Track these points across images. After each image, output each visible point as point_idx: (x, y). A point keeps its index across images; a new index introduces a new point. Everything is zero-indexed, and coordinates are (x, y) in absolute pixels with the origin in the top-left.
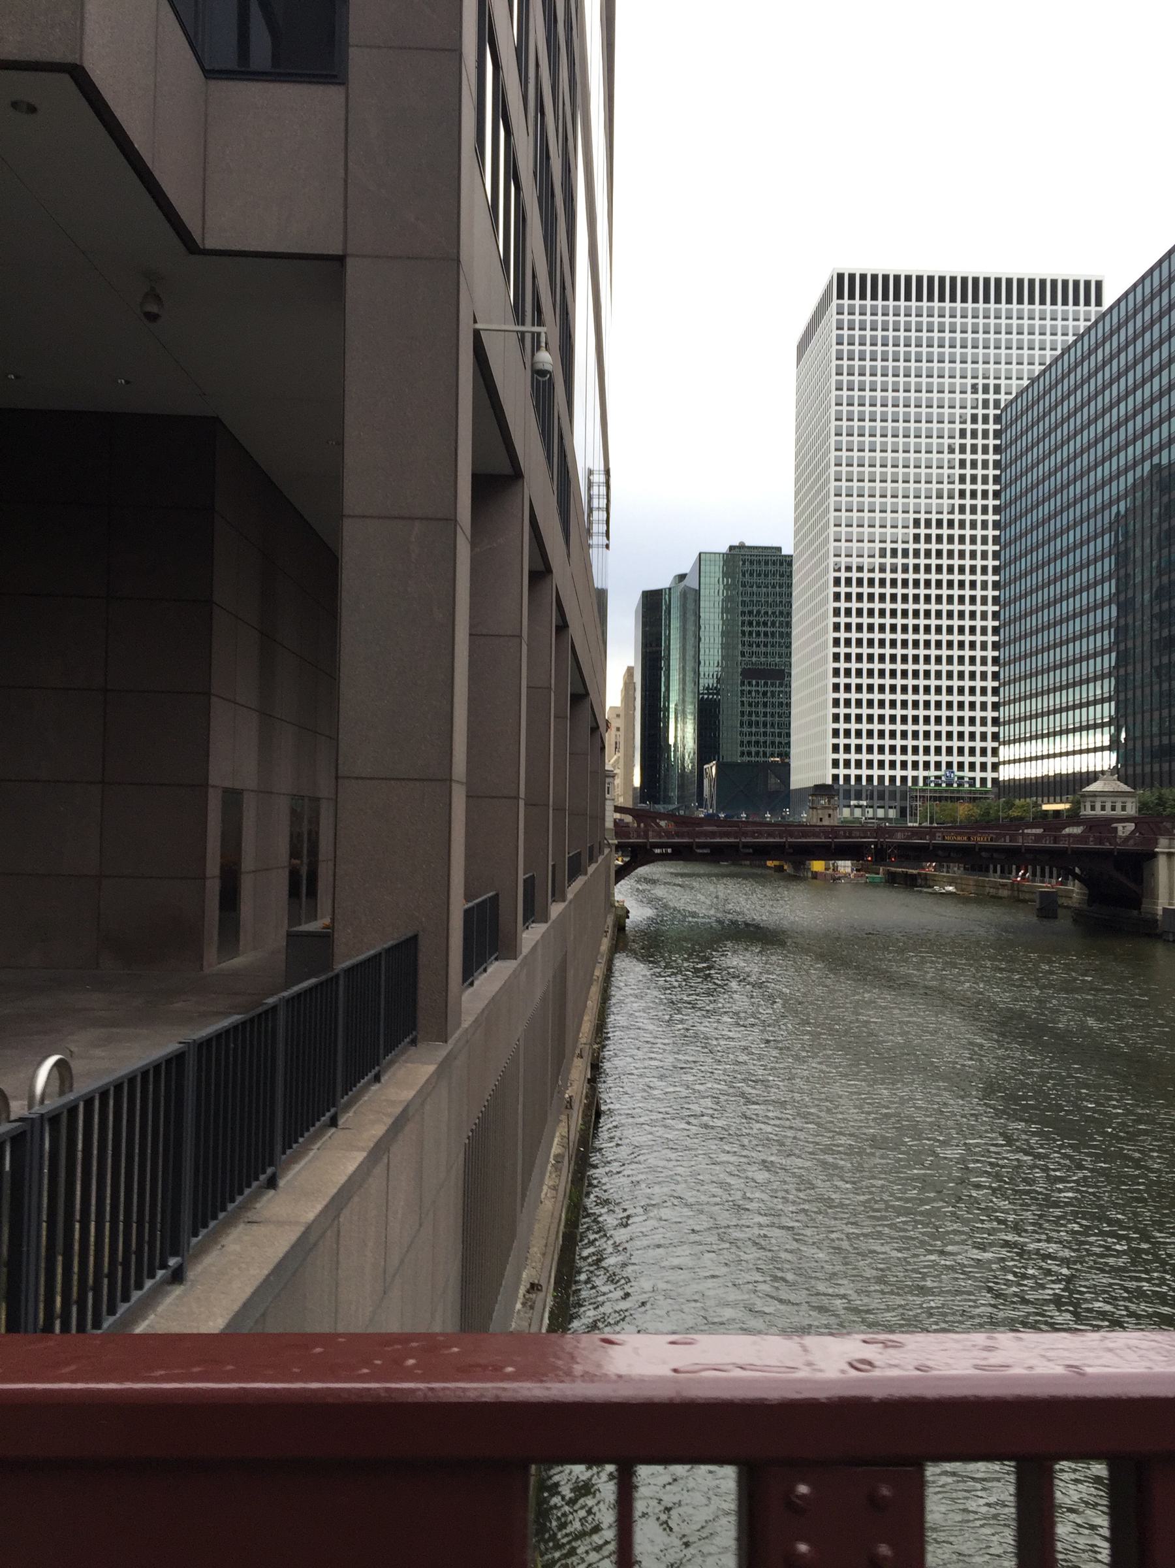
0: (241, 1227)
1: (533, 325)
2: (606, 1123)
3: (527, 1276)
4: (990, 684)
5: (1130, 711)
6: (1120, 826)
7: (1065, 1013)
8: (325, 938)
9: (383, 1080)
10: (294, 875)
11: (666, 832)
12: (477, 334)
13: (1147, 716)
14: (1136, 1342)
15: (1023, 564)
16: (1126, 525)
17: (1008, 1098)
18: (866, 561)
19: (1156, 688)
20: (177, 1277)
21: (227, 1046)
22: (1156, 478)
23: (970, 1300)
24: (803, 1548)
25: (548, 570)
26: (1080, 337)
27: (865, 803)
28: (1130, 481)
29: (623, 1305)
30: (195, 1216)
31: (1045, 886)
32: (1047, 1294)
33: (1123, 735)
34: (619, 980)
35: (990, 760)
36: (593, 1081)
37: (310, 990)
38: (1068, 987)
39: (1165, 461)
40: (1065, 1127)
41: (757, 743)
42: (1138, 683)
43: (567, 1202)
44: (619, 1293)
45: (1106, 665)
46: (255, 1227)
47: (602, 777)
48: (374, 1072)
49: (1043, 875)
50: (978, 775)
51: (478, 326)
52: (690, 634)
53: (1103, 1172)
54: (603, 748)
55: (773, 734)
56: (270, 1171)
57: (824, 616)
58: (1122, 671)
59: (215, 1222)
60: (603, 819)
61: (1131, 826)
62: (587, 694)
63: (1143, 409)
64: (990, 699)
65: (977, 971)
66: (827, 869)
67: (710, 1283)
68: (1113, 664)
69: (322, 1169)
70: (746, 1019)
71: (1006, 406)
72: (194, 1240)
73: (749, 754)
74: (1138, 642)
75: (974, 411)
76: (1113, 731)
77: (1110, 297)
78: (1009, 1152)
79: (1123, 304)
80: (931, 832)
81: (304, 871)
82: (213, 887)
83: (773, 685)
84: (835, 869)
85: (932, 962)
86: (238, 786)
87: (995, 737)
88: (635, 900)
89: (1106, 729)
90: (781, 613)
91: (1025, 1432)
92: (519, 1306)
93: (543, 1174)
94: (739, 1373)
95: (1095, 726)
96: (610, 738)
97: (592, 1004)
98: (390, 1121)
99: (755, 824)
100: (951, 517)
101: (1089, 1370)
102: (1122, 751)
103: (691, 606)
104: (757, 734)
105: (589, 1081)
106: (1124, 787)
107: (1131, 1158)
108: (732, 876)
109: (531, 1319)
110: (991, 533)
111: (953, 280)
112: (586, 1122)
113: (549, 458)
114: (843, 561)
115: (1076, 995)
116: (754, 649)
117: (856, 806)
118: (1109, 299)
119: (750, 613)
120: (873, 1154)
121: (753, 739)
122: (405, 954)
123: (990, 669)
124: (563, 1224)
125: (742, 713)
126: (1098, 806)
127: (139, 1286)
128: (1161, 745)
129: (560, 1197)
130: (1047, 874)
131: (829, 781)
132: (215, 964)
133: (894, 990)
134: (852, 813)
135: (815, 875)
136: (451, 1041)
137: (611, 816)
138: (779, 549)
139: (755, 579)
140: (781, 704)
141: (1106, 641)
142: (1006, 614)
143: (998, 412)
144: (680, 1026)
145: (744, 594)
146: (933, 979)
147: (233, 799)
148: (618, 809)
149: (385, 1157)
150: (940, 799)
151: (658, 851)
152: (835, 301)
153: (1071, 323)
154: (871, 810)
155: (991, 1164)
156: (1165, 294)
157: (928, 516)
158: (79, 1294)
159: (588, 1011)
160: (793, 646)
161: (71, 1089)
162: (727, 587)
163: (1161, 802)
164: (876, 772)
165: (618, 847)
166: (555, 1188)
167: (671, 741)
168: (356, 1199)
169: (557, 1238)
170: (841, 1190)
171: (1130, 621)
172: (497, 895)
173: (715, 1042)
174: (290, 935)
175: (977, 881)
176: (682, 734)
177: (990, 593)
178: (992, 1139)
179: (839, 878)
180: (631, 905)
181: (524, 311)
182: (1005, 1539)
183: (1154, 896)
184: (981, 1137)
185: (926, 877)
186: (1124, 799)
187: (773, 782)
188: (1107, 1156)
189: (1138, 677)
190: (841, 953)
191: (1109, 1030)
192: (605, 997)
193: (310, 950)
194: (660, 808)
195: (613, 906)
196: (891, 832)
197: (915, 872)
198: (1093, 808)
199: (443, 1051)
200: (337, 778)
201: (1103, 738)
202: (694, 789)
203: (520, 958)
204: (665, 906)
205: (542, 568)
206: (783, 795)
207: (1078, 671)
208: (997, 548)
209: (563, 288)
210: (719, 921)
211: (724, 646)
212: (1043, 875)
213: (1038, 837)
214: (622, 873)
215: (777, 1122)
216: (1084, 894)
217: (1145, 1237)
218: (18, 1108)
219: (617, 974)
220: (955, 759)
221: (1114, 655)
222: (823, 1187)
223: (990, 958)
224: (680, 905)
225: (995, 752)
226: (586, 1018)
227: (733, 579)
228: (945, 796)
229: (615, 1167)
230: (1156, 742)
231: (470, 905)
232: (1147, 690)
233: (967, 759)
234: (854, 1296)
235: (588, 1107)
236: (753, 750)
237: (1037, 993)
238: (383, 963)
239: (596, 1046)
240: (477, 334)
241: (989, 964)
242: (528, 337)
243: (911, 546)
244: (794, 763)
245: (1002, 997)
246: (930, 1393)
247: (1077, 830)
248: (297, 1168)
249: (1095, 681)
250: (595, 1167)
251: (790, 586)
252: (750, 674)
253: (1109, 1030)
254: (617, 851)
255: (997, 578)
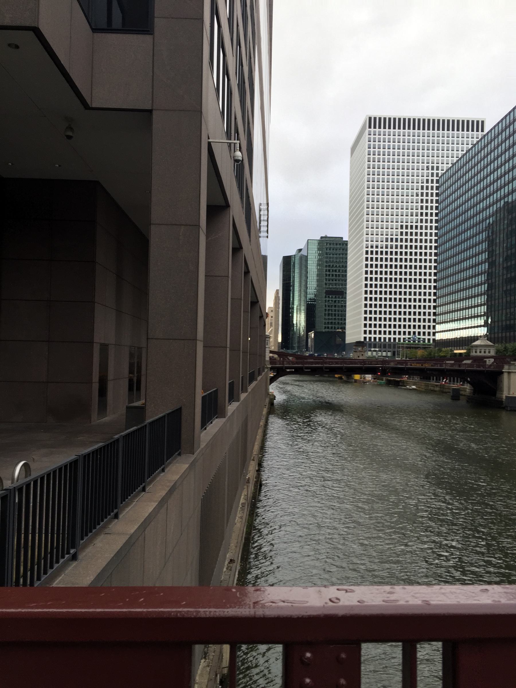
0: (102, 536)
1: (235, 140)
2: (264, 489)
3: (229, 556)
4: (433, 297)
5: (493, 309)
6: (487, 360)
7: (462, 441)
8: (142, 409)
9: (166, 471)
10: (131, 381)
11: (292, 362)
12: (209, 144)
13: (500, 312)
14: (454, 590)
15: (448, 245)
16: (493, 228)
17: (437, 479)
18: (379, 243)
19: (504, 300)
20: (74, 557)
21: (97, 456)
22: (506, 208)
23: (418, 566)
24: (308, 680)
25: (241, 248)
26: (474, 145)
27: (377, 349)
28: (495, 209)
29: (271, 568)
30: (82, 530)
31: (455, 386)
32: (451, 563)
33: (490, 320)
34: (270, 427)
35: (432, 331)
36: (259, 471)
37: (134, 432)
38: (464, 430)
39: (510, 200)
40: (460, 490)
41: (332, 323)
42: (497, 297)
43: (246, 524)
44: (268, 563)
45: (483, 290)
46: (108, 536)
47: (264, 338)
48: (162, 468)
49: (454, 381)
50: (427, 337)
51: (210, 140)
52: (303, 275)
53: (477, 511)
54: (265, 325)
55: (338, 319)
56: (115, 511)
57: (361, 268)
58: (490, 293)
59: (91, 534)
60: (265, 356)
61: (492, 360)
62: (258, 302)
63: (501, 177)
64: (432, 304)
65: (425, 422)
66: (361, 378)
67: (307, 559)
68: (486, 289)
69: (139, 510)
70: (325, 444)
71: (441, 176)
72: (82, 542)
73: (328, 328)
74: (497, 279)
75: (428, 178)
76: (485, 319)
77: (487, 128)
78: (436, 501)
79: (493, 131)
80: (405, 362)
81: (135, 379)
82: (96, 386)
83: (339, 298)
84: (364, 378)
85: (405, 419)
86: (106, 342)
87: (434, 320)
88: (278, 392)
89: (482, 318)
90: (343, 266)
91: (406, 629)
92: (225, 569)
93: (236, 511)
94: (282, 604)
95: (478, 316)
96: (268, 321)
97: (259, 437)
98: (168, 489)
99: (330, 358)
100: (417, 224)
101: (432, 602)
102: (489, 327)
103: (304, 262)
104: (331, 319)
105: (257, 471)
106: (490, 343)
107: (489, 505)
108: (320, 381)
109: (230, 575)
110: (434, 231)
111: (419, 120)
112: (255, 489)
113: (242, 198)
114: (370, 243)
115: (466, 432)
116: (331, 282)
117: (374, 351)
118: (487, 129)
119: (329, 266)
120: (378, 503)
121: (330, 321)
122: (176, 416)
123: (433, 291)
124: (244, 533)
125: (325, 310)
126: (478, 351)
127: (57, 562)
128: (506, 325)
129: (244, 521)
130: (456, 381)
131: (362, 340)
132: (96, 420)
133: (389, 431)
134: (372, 354)
135: (356, 381)
136: (196, 454)
137: (268, 355)
138: (342, 238)
139: (331, 251)
140: (342, 306)
141: (483, 279)
142: (440, 267)
143: (438, 178)
144: (297, 447)
145: (327, 258)
146: (405, 426)
147: (104, 348)
148: (271, 352)
149: (166, 505)
150: (410, 348)
151: (288, 370)
152: (368, 129)
153: (470, 139)
154: (380, 352)
155: (428, 507)
156: (512, 127)
157: (412, 224)
158: (31, 566)
159: (257, 440)
160: (348, 281)
161: (30, 475)
162: (319, 255)
163: (506, 349)
164: (397, 336)
165: (271, 369)
166: (241, 518)
167: (295, 322)
168: (152, 523)
169: (242, 539)
170: (363, 518)
171: (494, 270)
172: (217, 390)
173: (311, 454)
174: (128, 408)
175: (426, 384)
176: (299, 319)
177: (433, 258)
178: (429, 496)
179: (366, 382)
180: (276, 393)
181: (231, 133)
182: (398, 677)
183: (502, 391)
184: (424, 495)
185: (403, 382)
186: (489, 348)
187: (339, 340)
188: (479, 503)
189: (497, 295)
190: (367, 415)
191: (481, 449)
192: (265, 434)
193: (136, 414)
194: (290, 351)
195: (269, 394)
196: (388, 362)
197: (399, 380)
198: (476, 352)
199: (192, 458)
200: (147, 339)
201: (481, 321)
202: (304, 343)
203: (227, 417)
204: (291, 395)
205: (237, 246)
206: (342, 346)
207: (470, 292)
208: (436, 238)
209: (249, 123)
210: (314, 401)
211: (318, 281)
212: (454, 381)
213: (452, 365)
214: (273, 380)
215: (338, 489)
216: (471, 390)
217: (494, 539)
218: (7, 484)
219: (270, 424)
220: (417, 330)
221: (486, 285)
222: (356, 516)
223: (430, 417)
224: (297, 394)
225: (434, 327)
226: (256, 443)
227: (322, 251)
228: (412, 346)
229: (267, 508)
230: (504, 323)
231: (205, 394)
232: (501, 301)
233: (422, 330)
234: (368, 564)
235: (256, 482)
236: (330, 326)
237: (450, 432)
238: (166, 420)
239: (260, 456)
240: (209, 144)
241: (429, 420)
242: (232, 145)
243: (399, 237)
244: (348, 332)
245: (435, 435)
246: (363, 612)
247: (469, 362)
248: (127, 510)
249: (475, 298)
250: (258, 508)
251: (346, 254)
252: (329, 293)
253: (481, 449)
254: (271, 370)
255: (436, 251)
